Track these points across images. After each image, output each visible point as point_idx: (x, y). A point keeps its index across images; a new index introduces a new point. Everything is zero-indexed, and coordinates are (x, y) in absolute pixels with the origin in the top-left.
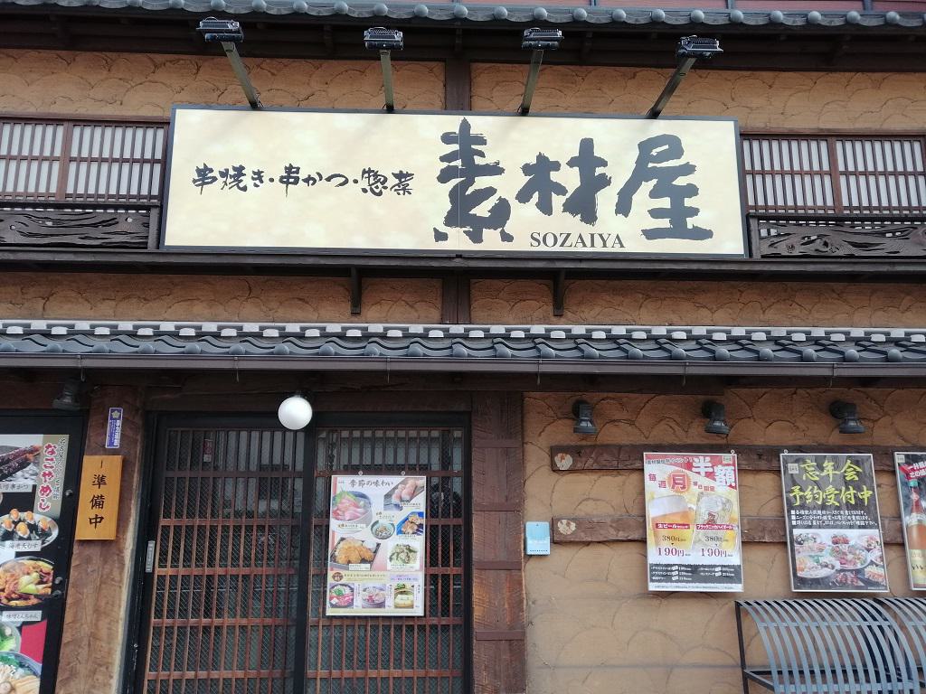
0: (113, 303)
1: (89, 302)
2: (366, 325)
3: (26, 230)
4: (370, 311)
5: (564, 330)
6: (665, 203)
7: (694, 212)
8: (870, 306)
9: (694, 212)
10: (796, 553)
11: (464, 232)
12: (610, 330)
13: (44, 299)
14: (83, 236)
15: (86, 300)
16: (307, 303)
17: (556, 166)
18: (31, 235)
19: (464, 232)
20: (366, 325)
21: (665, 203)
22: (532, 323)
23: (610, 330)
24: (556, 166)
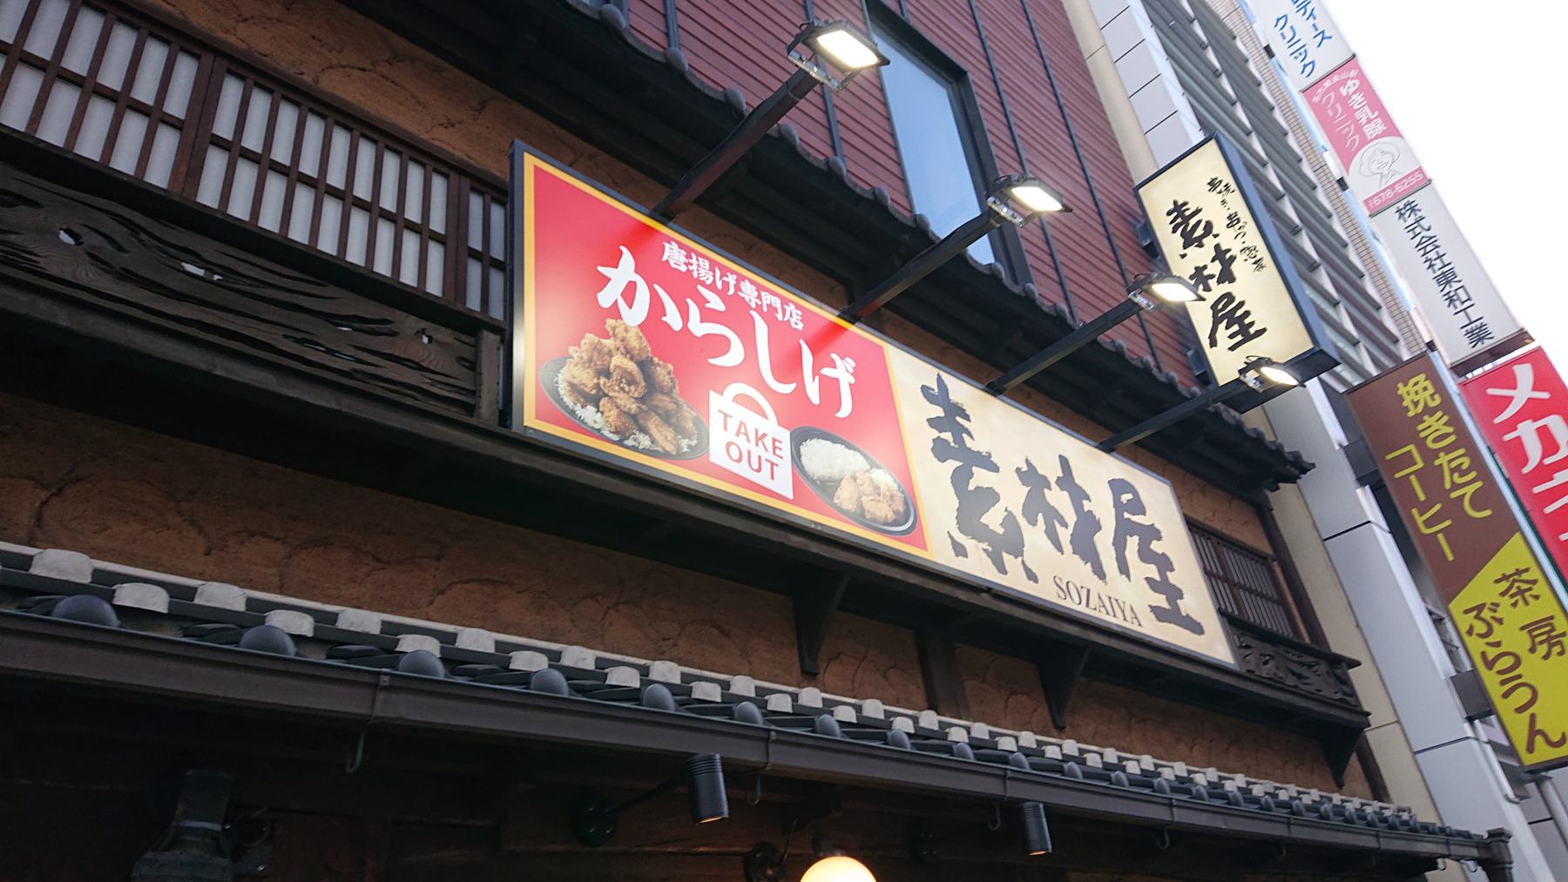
0: (278, 550)
1: (200, 530)
2: (647, 662)
3: (121, 260)
4: (830, 673)
5: (318, 615)
6: (1236, 328)
7: (1252, 324)
8: (802, 84)
9: (1252, 324)
10: (1269, 649)
11: (924, 548)
12: (455, 635)
13: (40, 484)
14: (299, 335)
15: (193, 523)
16: (727, 635)
17: (1205, 267)
18: (126, 276)
19: (924, 548)
20: (450, 628)
21: (1236, 328)
22: (660, 656)
23: (455, 635)
24: (1205, 267)
